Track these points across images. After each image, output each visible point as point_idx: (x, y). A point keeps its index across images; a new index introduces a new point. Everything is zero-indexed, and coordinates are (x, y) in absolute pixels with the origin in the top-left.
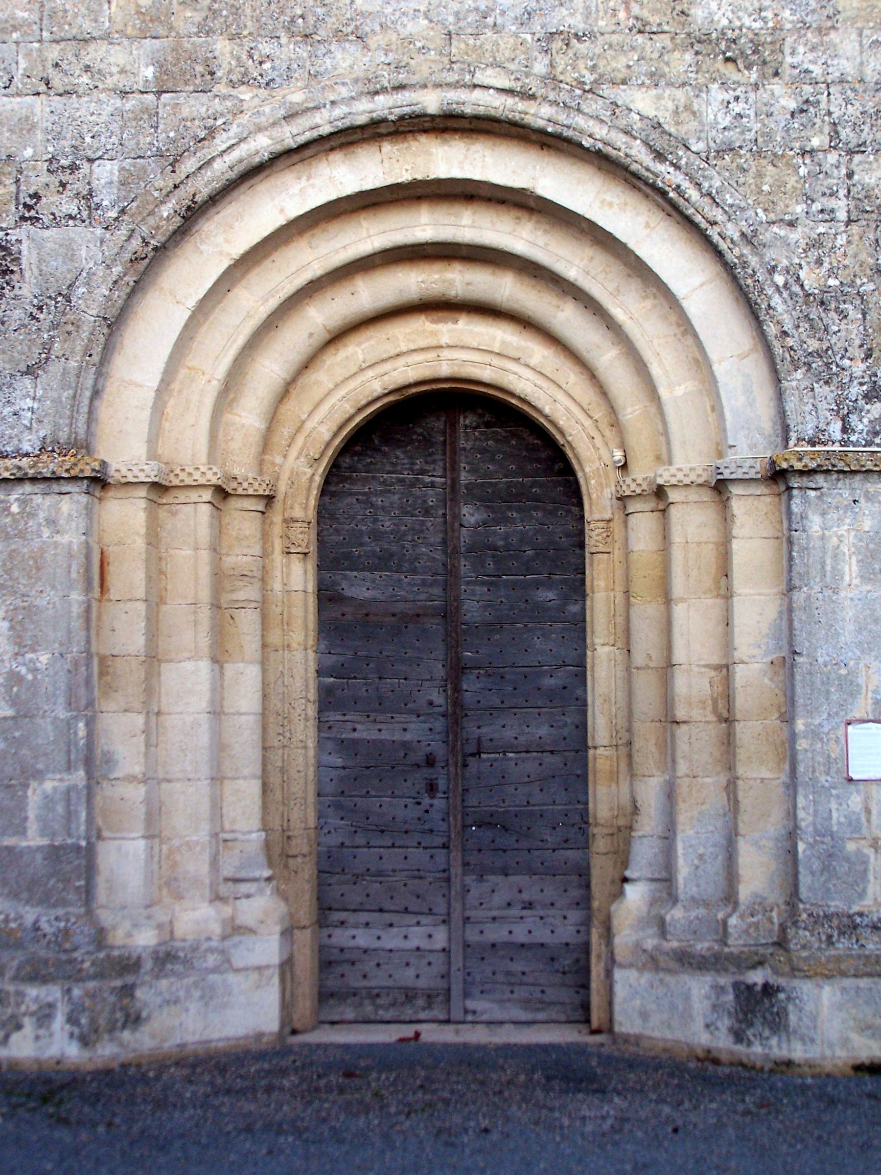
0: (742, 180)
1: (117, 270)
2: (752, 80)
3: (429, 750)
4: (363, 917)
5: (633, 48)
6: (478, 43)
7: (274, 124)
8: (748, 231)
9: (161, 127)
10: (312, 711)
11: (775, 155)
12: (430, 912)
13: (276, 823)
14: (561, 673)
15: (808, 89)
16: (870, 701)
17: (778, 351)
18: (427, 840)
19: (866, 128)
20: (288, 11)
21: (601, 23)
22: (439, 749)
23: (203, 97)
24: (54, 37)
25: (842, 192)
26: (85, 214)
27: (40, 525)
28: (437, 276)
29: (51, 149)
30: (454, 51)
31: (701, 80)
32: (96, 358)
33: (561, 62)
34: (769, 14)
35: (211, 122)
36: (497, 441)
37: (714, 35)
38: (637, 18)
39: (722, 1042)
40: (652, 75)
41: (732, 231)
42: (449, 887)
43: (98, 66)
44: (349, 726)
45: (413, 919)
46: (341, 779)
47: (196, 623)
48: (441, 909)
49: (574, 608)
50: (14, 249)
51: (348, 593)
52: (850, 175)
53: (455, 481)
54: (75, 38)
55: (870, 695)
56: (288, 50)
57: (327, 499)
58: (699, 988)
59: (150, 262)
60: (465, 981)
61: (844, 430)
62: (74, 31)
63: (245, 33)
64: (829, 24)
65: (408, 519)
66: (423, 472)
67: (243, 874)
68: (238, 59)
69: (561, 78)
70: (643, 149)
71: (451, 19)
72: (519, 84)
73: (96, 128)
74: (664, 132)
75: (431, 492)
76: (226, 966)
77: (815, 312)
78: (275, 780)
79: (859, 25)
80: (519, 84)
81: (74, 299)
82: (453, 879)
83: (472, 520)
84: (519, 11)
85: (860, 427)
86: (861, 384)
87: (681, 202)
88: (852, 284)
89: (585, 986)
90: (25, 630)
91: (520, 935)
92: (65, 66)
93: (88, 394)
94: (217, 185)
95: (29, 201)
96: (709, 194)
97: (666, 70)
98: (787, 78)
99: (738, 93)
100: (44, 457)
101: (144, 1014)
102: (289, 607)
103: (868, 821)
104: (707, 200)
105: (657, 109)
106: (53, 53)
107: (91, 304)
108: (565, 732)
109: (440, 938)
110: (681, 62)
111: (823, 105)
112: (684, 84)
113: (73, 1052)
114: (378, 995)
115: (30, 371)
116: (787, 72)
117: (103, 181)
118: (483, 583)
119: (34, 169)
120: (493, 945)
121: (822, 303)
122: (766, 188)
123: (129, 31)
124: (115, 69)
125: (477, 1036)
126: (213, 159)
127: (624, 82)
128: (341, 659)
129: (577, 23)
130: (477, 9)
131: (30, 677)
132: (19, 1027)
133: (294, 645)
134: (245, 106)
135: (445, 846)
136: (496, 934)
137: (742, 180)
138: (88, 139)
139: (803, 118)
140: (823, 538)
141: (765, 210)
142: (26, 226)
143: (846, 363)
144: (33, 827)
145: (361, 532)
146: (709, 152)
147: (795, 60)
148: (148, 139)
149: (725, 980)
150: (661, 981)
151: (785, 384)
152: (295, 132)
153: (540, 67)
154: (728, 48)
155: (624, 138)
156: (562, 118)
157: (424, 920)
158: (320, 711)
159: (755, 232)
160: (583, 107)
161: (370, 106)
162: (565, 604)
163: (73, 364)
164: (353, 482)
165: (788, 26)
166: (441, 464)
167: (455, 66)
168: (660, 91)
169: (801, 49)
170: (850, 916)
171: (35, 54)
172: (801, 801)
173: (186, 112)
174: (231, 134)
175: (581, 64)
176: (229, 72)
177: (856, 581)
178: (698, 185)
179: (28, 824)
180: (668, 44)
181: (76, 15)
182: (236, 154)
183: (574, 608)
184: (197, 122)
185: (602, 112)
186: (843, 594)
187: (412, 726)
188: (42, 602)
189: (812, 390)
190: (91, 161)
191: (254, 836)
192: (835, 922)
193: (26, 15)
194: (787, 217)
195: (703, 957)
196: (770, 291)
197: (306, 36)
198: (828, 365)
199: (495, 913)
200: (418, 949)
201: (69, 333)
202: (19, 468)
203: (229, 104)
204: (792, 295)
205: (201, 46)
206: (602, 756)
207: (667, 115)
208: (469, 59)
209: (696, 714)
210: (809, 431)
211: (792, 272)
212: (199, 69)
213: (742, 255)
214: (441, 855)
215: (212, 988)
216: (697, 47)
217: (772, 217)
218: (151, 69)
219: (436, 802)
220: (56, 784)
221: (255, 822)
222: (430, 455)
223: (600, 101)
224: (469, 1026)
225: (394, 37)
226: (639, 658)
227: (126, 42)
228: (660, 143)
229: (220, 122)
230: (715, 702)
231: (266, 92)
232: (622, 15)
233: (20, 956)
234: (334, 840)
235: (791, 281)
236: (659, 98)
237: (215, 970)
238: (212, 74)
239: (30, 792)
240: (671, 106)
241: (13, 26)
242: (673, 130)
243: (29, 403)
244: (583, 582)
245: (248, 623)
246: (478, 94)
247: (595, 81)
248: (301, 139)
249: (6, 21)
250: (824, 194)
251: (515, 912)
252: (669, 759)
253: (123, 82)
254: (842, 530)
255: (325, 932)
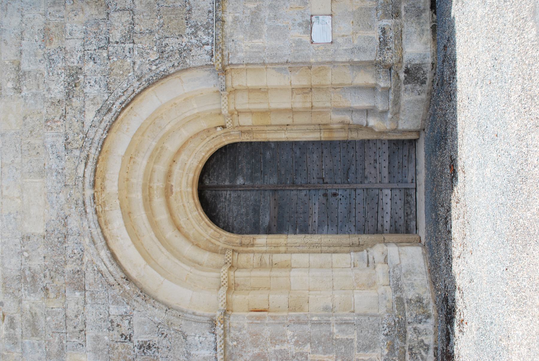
0: (118, 81)
1: (149, 306)
2: (83, 77)
3: (322, 195)
4: (380, 219)
5: (71, 120)
6: (68, 175)
7: (97, 249)
8: (137, 79)
9: (97, 290)
10: (308, 236)
11: (109, 69)
12: (378, 195)
13: (348, 249)
14: (295, 150)
15: (86, 57)
16: (304, 35)
17: (179, 68)
18: (353, 196)
19: (100, 37)
20: (56, 244)
21: (62, 131)
22: (321, 193)
23: (87, 274)
24: (65, 328)
25: (123, 45)
26: (129, 317)
27: (241, 334)
28: (155, 192)
29: (105, 330)
30: (71, 184)
31: (83, 95)
32: (181, 314)
33: (76, 146)
34: (59, 71)
35: (96, 272)
36: (214, 172)
37: (67, 91)
38: (60, 118)
39: (427, 87)
40: (80, 113)
41: (136, 84)
42: (370, 188)
43: (75, 312)
44: (313, 223)
45: (380, 201)
46: (332, 226)
47: (277, 277)
48: (377, 191)
49: (273, 145)
50: (141, 343)
51: (267, 224)
52: (117, 43)
53: (228, 186)
54: (65, 321)
55: (302, 35)
56: (70, 243)
57: (235, 231)
58: (406, 97)
59: (145, 295)
60: (402, 183)
61: (208, 45)
62: (63, 321)
63: (64, 259)
64: (63, 50)
65: (242, 203)
66: (225, 198)
67: (366, 260)
68: (73, 262)
69: (81, 145)
70: (107, 116)
71: (59, 185)
72: (83, 160)
73: (98, 313)
74: (101, 109)
75: (232, 195)
76: (399, 266)
77: (166, 55)
78: (332, 249)
79: (64, 40)
80: (83, 160)
81: (159, 322)
82: (367, 187)
83: (242, 181)
84: (57, 161)
85: (206, 39)
86: (191, 38)
87: (126, 103)
88: (156, 42)
89: (403, 141)
90: (279, 340)
91: (386, 164)
92: (75, 325)
93: (194, 316)
94: (119, 270)
95: (124, 338)
96: (123, 93)
97: (79, 108)
98: (82, 65)
99: (87, 82)
100: (217, 332)
101: (417, 296)
102: (272, 244)
103: (347, 36)
104: (125, 93)
105: (93, 111)
106: (71, 329)
107: (159, 315)
108: (315, 148)
109: (388, 192)
110: (76, 103)
111: (92, 52)
112: (84, 102)
113: (431, 321)
114: (407, 213)
115: (185, 338)
116: (80, 65)
117: (117, 311)
118: (264, 177)
119: (112, 336)
120: (389, 173)
121: (162, 52)
122: (121, 72)
123: (63, 301)
124: (77, 306)
125: (422, 178)
126: (109, 271)
127: (83, 123)
128: (290, 226)
129: (62, 139)
130: (56, 175)
131: (296, 338)
132: (422, 341)
133: (285, 242)
134: (90, 259)
135: (355, 190)
136: (385, 172)
137: (118, 81)
138: (102, 316)
139: (97, 59)
140: (246, 52)
141: (129, 73)
142: (133, 339)
143: (184, 44)
144: (350, 337)
145: (247, 219)
146: (108, 93)
147: (76, 62)
148: (102, 294)
149: (403, 87)
150: (403, 111)
151: (191, 66)
152: (100, 241)
153: (77, 153)
154: (71, 86)
155: (103, 123)
156: (95, 145)
157: (381, 197)
158: (308, 234)
159: (137, 76)
160: (92, 138)
161: (91, 214)
162: (271, 148)
163: (183, 322)
164: (229, 222)
165: (64, 64)
166: (223, 192)
167: (77, 183)
168: (86, 110)
169: (72, 60)
170: (380, 42)
171: (71, 335)
172: (340, 60)
173: (92, 281)
174: (100, 264)
175: (76, 138)
176: (78, 265)
177: (261, 40)
178: (120, 96)
179: (349, 338)
180: (69, 107)
181: (57, 320)
182: (107, 263)
183: (273, 145)
184: (96, 277)
185: (93, 131)
186: (266, 45)
187: (313, 202)
188: (269, 334)
189: (193, 56)
190: (109, 315)
191: (352, 256)
192: (383, 47)
193: (57, 338)
194: (132, 65)
195: (395, 96)
196: (158, 71)
197: (65, 237)
198: (184, 50)
199: (378, 173)
200: (391, 199)
201: (172, 323)
202: (221, 341)
203: (89, 265)
204: (159, 63)
205: (68, 275)
206: (323, 136)
207: (95, 107)
208: (74, 178)
209: (309, 100)
210: (208, 57)
211: (152, 63)
212: (76, 276)
213: (145, 81)
214: (358, 191)
215: (407, 271)
216: (71, 97)
217: (131, 70)
218: (76, 293)
219: (340, 193)
220: (334, 328)
221: (348, 255)
222: (219, 195)
223: (90, 131)
224: (417, 181)
225: (66, 205)
226: (289, 121)
227: (67, 302)
228: (105, 110)
229: (96, 269)
230: (305, 93)
231: (85, 252)
232: (59, 124)
233: (397, 341)
234: (353, 229)
235: (155, 63)
236: (88, 110)
237: (401, 271)
238: (78, 271)
239: (338, 338)
240: (92, 106)
241: (61, 343)
242: (100, 106)
243: (197, 338)
244: (264, 142)
245: (277, 258)
246: (86, 175)
247: (82, 133)
248: (103, 239)
249: (59, 345)
250: (124, 52)
251: (378, 166)
252: (325, 110)
253: (81, 302)
254: (243, 45)
255: (385, 231)
